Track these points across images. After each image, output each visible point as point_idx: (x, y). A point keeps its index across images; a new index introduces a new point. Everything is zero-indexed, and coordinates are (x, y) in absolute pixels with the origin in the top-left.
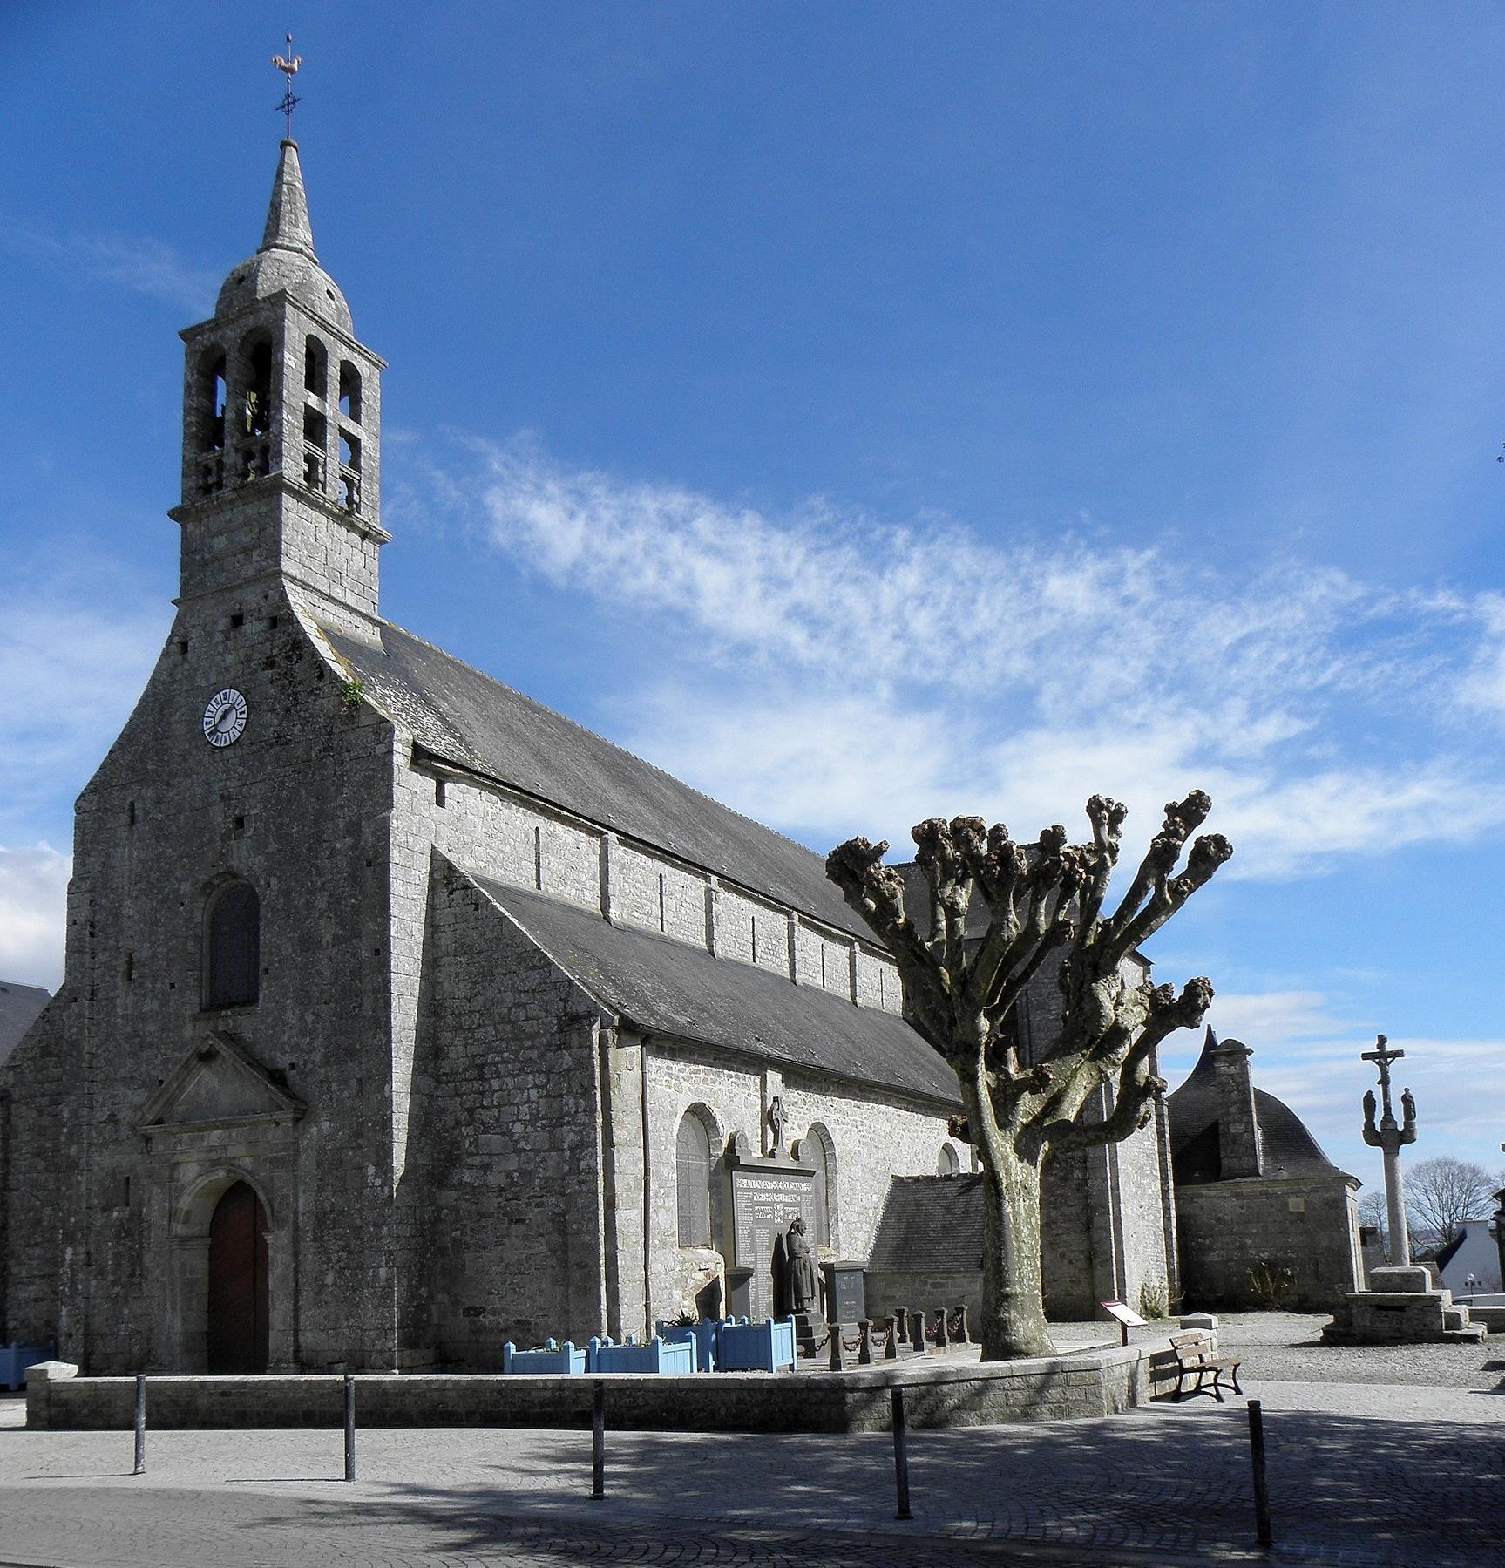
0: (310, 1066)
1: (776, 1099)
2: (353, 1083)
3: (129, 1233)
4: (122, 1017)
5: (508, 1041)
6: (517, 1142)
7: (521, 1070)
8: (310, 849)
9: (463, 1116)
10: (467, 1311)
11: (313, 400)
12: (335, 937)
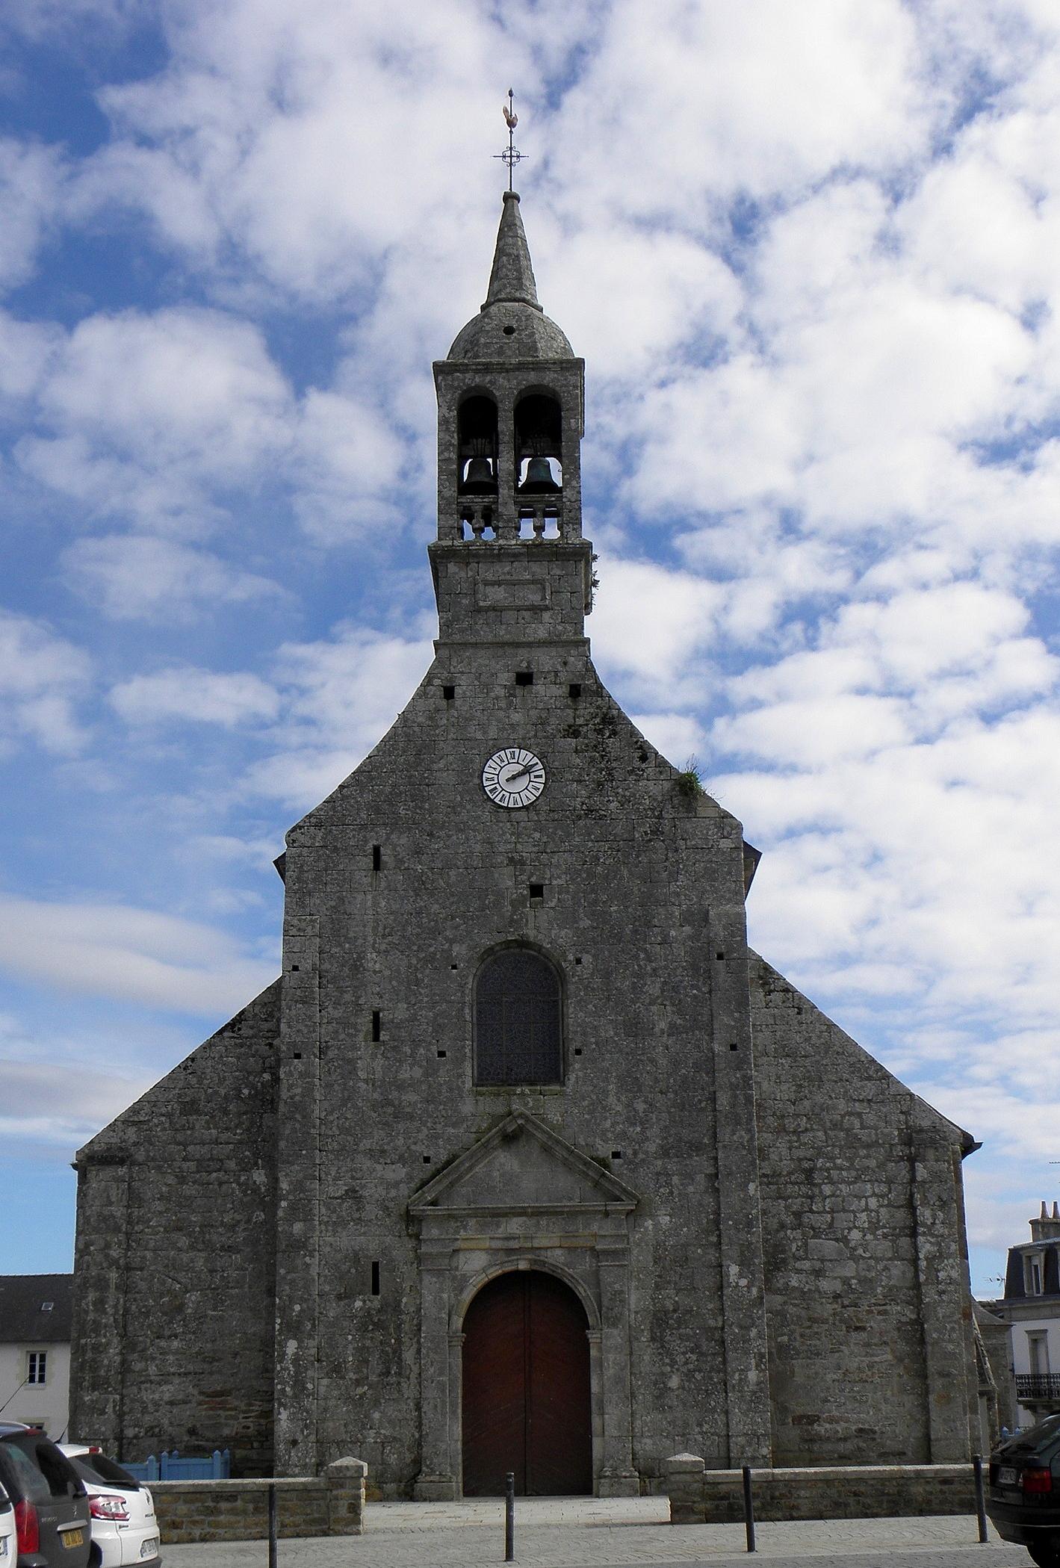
0: (641, 1156)
3: (378, 1326)
4: (366, 1081)
5: (841, 1147)
6: (854, 1249)
7: (858, 1178)
8: (635, 931)
9: (789, 1220)
10: (798, 1420)
12: (672, 1026)
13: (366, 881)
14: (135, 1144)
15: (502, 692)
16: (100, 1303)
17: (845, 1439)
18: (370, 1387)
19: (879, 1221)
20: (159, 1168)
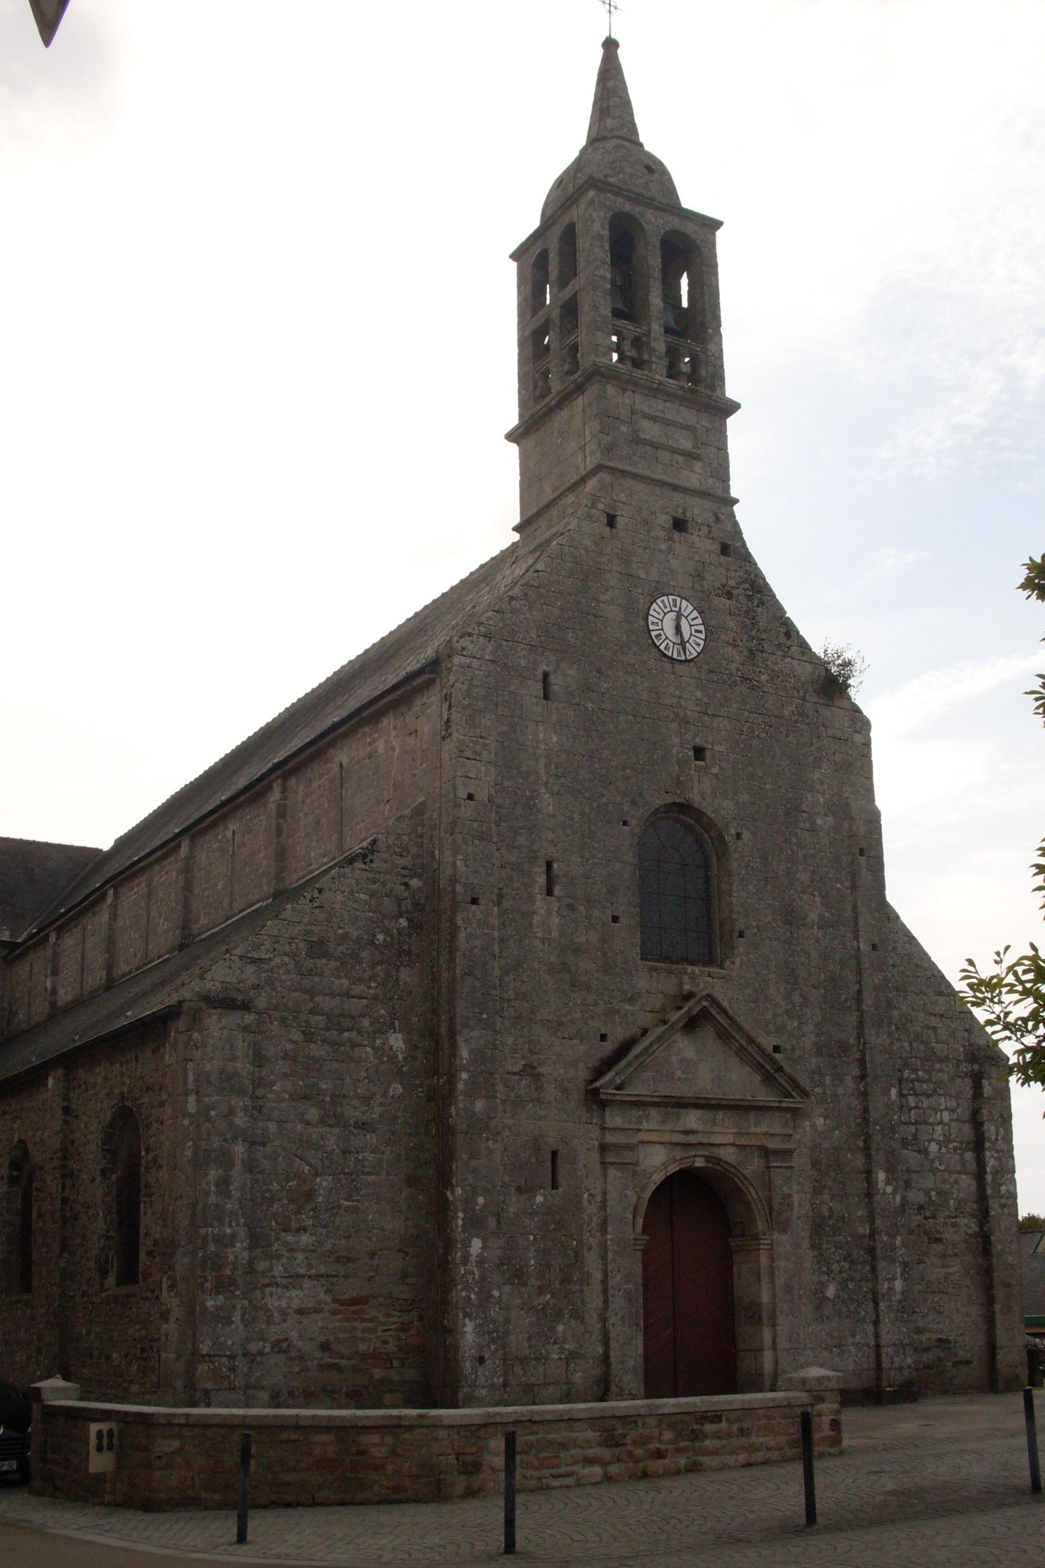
0: (797, 1052)
6: (933, 1161)
7: (935, 1091)
13: (538, 709)
14: (256, 987)
15: (662, 534)
16: (223, 1183)
17: (927, 1349)
18: (553, 1294)
19: (950, 1135)
20: (283, 1020)
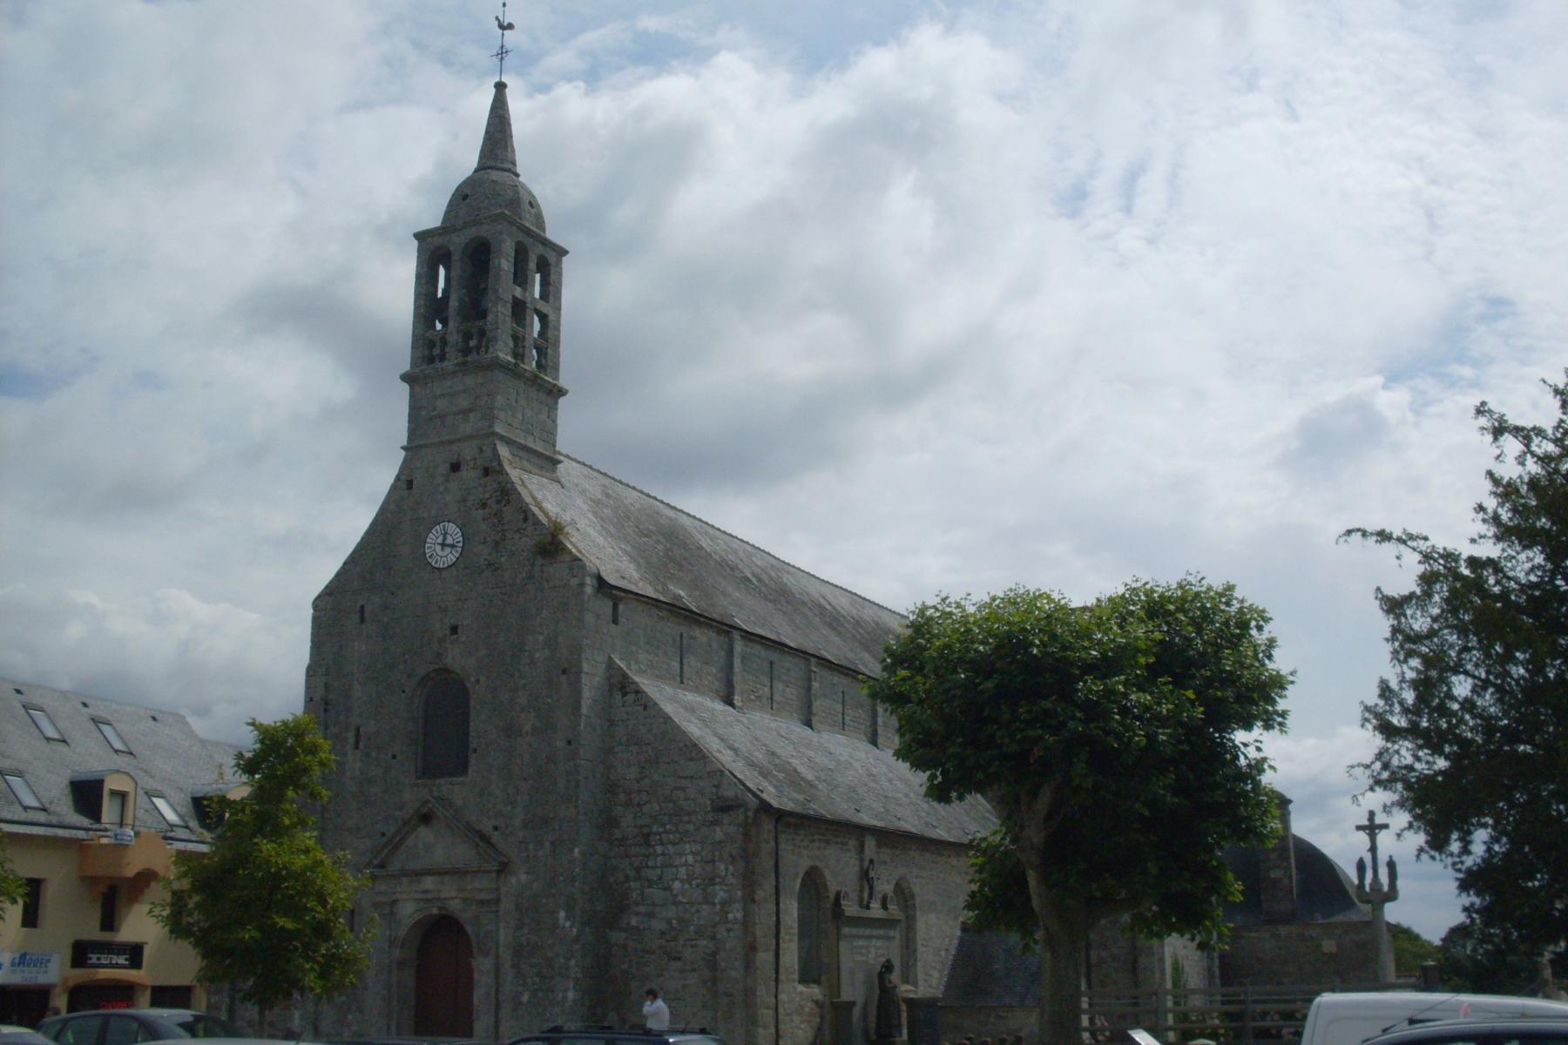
1: (871, 861)
2: (547, 844)
7: (681, 840)
9: (632, 874)
11: (518, 292)
